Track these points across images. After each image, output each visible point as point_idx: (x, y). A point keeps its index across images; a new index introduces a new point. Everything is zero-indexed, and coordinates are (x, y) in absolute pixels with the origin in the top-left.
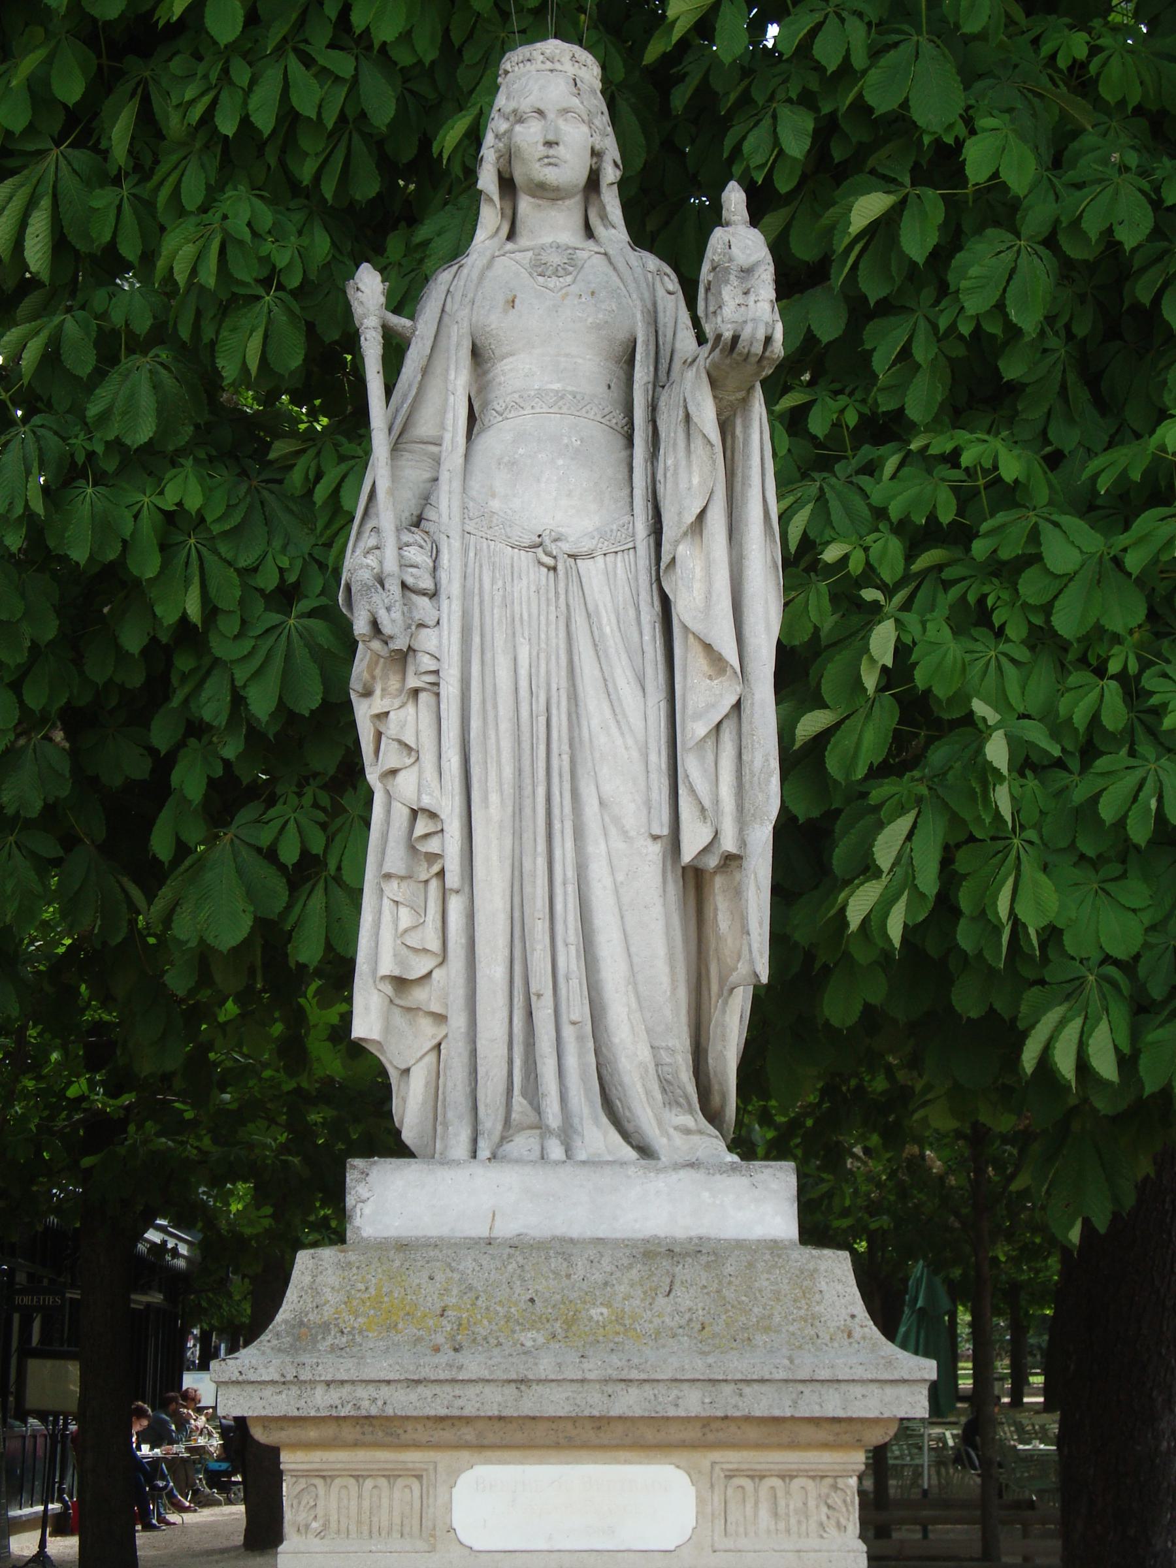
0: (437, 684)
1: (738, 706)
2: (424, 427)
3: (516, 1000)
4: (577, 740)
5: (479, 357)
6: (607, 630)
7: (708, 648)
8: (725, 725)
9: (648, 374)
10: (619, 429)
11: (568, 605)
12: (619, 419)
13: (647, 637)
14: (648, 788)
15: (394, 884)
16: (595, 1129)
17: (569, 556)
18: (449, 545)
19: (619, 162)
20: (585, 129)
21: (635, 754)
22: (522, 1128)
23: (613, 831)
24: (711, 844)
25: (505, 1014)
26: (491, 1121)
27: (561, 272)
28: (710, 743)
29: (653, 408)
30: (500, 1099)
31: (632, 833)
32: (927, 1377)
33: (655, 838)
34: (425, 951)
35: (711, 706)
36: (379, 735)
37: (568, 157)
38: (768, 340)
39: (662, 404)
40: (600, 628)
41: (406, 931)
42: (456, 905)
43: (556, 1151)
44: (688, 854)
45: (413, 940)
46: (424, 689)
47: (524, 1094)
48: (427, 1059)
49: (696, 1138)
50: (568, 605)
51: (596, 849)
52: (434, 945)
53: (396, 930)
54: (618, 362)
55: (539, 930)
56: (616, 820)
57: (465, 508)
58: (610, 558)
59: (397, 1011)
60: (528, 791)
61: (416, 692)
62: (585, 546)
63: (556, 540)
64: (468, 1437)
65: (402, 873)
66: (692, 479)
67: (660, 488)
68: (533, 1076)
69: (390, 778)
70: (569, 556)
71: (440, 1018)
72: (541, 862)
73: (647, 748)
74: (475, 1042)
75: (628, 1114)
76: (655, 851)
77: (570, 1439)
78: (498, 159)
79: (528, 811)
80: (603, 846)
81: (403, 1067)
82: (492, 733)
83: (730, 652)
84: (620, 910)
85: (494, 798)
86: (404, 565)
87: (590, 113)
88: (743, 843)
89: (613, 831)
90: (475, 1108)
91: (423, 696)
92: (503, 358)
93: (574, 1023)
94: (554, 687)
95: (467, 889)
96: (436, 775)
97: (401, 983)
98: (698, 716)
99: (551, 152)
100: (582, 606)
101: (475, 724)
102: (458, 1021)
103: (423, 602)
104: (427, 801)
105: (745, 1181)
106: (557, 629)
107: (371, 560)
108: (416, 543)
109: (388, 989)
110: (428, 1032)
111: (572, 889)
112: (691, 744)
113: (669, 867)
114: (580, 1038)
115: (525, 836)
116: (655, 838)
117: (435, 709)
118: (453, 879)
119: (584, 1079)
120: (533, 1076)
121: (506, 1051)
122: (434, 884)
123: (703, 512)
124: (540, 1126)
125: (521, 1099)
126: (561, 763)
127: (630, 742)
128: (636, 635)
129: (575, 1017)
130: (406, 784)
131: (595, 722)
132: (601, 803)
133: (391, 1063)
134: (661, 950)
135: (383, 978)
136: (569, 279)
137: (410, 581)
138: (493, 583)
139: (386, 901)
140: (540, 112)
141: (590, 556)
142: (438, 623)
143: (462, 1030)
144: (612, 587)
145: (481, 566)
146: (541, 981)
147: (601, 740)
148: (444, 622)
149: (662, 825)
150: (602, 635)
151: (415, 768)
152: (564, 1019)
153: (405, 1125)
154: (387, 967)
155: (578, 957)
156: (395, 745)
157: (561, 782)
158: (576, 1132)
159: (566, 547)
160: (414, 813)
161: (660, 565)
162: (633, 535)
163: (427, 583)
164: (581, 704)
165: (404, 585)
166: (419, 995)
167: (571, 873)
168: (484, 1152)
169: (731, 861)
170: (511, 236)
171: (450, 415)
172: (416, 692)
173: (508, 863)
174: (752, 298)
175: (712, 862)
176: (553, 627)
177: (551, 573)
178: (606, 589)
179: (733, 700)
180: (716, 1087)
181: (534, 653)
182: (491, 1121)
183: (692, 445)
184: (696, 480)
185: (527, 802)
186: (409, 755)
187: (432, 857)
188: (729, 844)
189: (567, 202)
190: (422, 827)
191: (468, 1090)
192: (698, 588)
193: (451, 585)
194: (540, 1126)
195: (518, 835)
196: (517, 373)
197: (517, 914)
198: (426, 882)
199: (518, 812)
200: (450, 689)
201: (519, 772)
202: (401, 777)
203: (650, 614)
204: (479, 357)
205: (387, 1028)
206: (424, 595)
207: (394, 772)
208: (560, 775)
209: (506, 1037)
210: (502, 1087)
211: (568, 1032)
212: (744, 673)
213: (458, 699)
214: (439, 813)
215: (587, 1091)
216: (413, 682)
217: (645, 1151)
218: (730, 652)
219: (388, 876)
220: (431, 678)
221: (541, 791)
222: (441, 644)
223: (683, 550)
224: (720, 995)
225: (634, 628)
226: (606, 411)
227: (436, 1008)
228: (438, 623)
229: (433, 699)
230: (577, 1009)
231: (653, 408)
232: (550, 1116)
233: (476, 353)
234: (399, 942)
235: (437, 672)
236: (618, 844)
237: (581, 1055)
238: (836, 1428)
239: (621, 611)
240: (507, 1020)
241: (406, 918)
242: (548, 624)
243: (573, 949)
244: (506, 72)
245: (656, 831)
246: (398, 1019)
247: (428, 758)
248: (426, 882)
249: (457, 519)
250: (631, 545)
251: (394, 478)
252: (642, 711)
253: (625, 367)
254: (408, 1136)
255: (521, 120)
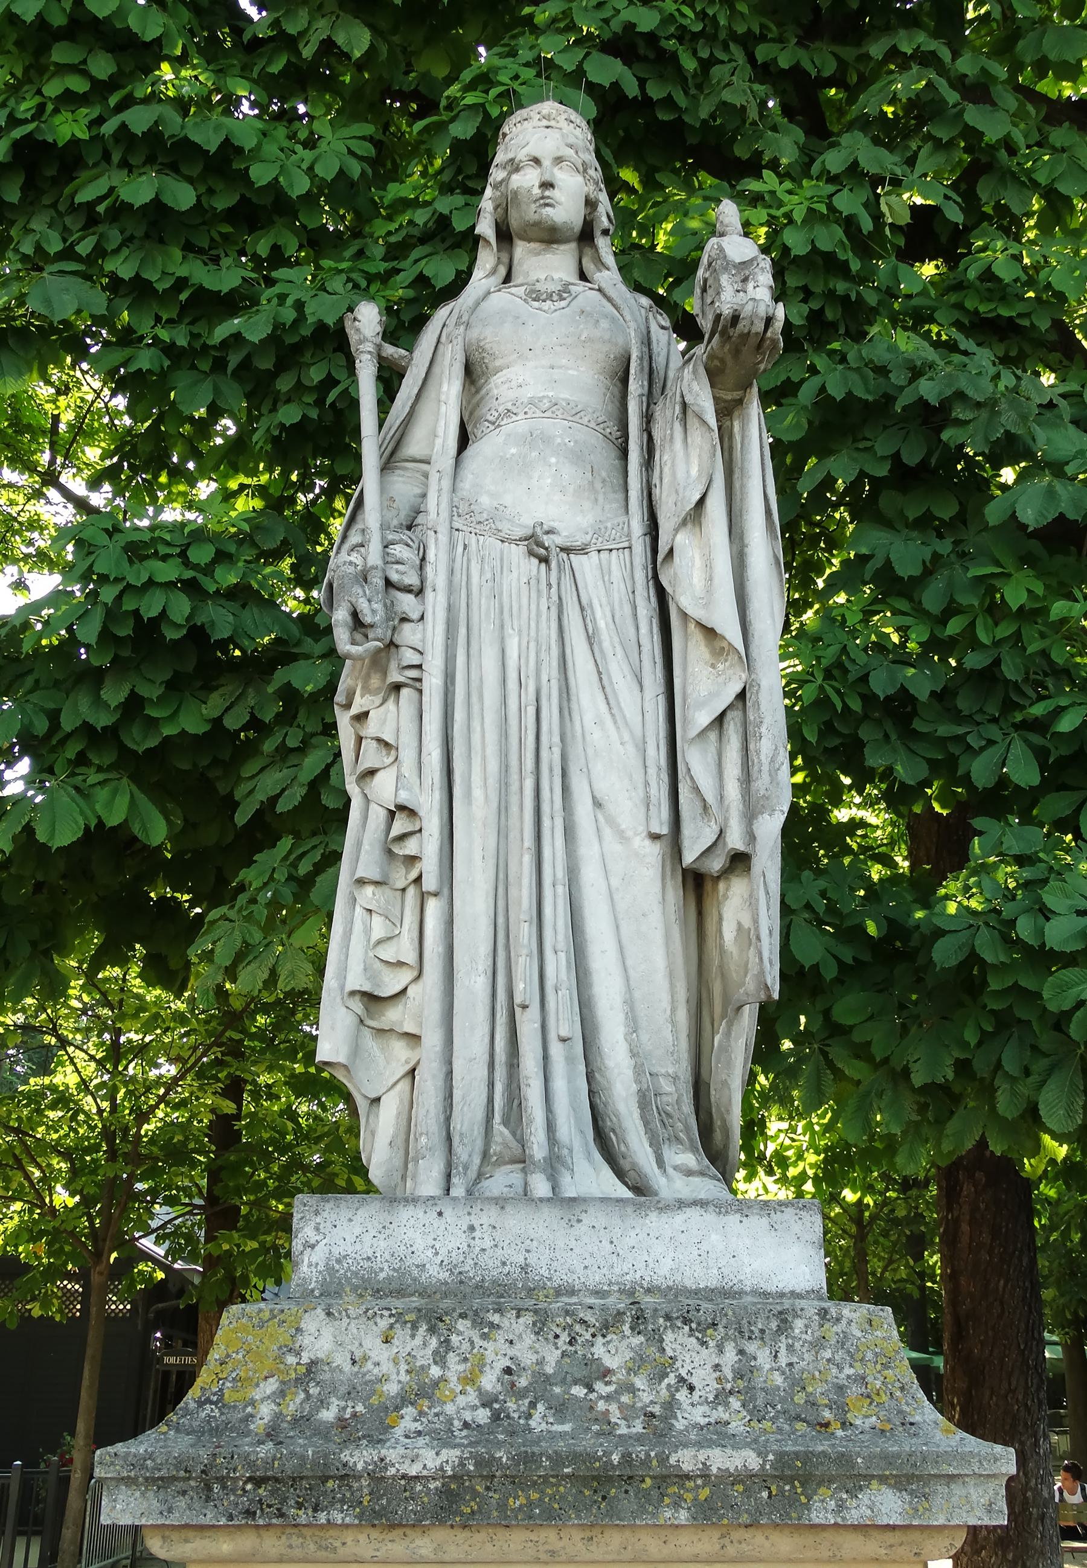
0: (420, 680)
1: (742, 696)
2: (414, 447)
3: (498, 1015)
4: (569, 734)
5: (473, 373)
6: (601, 624)
7: (710, 633)
8: (730, 715)
9: (642, 386)
10: (613, 438)
11: (560, 598)
12: (613, 429)
13: (644, 630)
14: (647, 784)
15: (369, 890)
16: (586, 1164)
17: (562, 549)
18: (436, 540)
19: (612, 214)
20: (580, 179)
21: (631, 749)
22: (501, 1162)
23: (607, 832)
24: (715, 844)
25: (486, 1029)
26: (467, 1152)
27: (555, 297)
28: (713, 736)
29: (648, 419)
30: (478, 1132)
31: (630, 833)
32: (1004, 1470)
33: (655, 837)
34: (400, 964)
35: (713, 695)
36: (360, 740)
37: (563, 199)
38: (769, 321)
39: (657, 415)
40: (594, 620)
41: (379, 942)
42: (433, 907)
43: (541, 1187)
44: (689, 857)
45: (388, 953)
46: (405, 685)
47: (506, 1122)
48: (399, 1087)
49: (696, 1180)
50: (560, 598)
51: (588, 850)
52: (411, 957)
53: (369, 941)
54: (612, 378)
55: (524, 933)
56: (611, 822)
57: (453, 506)
58: (604, 555)
59: (366, 1032)
60: (515, 787)
61: (397, 687)
62: (579, 540)
63: (547, 533)
64: (423, 1552)
65: (377, 877)
66: (686, 464)
67: (656, 492)
68: (516, 1102)
69: (368, 780)
70: (562, 549)
71: (413, 1039)
72: (528, 859)
73: (645, 742)
74: (451, 1063)
75: (623, 1148)
76: (654, 852)
77: (552, 1553)
78: (496, 209)
79: (514, 809)
80: (596, 847)
81: (373, 1095)
82: (476, 725)
83: (732, 633)
84: (616, 918)
85: (478, 793)
86: (388, 560)
87: (584, 163)
88: (751, 837)
89: (607, 832)
90: (449, 1139)
91: (405, 692)
92: (498, 370)
93: (564, 1040)
94: (544, 678)
95: (446, 891)
96: (415, 772)
97: (372, 1000)
98: (701, 705)
99: (547, 193)
100: (575, 598)
101: (459, 715)
102: (432, 1039)
103: (409, 598)
104: (404, 797)
105: (765, 1221)
106: (548, 620)
107: (355, 557)
108: (401, 542)
109: (357, 1005)
110: (401, 1055)
111: (561, 890)
112: (693, 732)
113: (669, 873)
114: (570, 1060)
115: (511, 835)
116: (655, 837)
117: (417, 705)
118: (430, 883)
119: (574, 1107)
120: (516, 1102)
121: (486, 1073)
122: (411, 891)
123: (701, 502)
124: (522, 1160)
125: (502, 1128)
126: (551, 756)
127: (626, 737)
128: (632, 631)
129: (564, 1033)
130: (385, 788)
131: (589, 718)
132: (597, 804)
133: (359, 1091)
134: (659, 960)
135: (353, 993)
136: (563, 303)
137: (394, 577)
138: (482, 572)
139: (358, 909)
140: (537, 161)
141: (583, 550)
142: (422, 618)
143: (438, 1049)
144: (609, 583)
145: (469, 560)
146: (525, 988)
147: (596, 736)
148: (429, 617)
149: (661, 824)
150: (596, 628)
151: (395, 768)
152: (552, 1036)
153: (374, 1161)
154: (356, 981)
155: (568, 967)
156: (374, 744)
157: (551, 776)
158: (564, 1164)
159: (559, 540)
160: (392, 814)
161: (658, 556)
162: (629, 535)
163: (412, 579)
164: (573, 698)
165: (388, 583)
166: (392, 1016)
167: (561, 874)
168: (458, 1191)
169: (740, 861)
170: (507, 279)
171: (442, 423)
172: (397, 687)
173: (492, 862)
174: (750, 285)
175: (716, 864)
176: (544, 617)
177: (543, 565)
178: (600, 583)
179: (738, 688)
180: (718, 1123)
181: (524, 644)
182: (467, 1152)
183: (689, 440)
184: (694, 471)
185: (514, 800)
186: (388, 754)
187: (412, 860)
188: (735, 841)
189: (562, 247)
190: (400, 826)
191: (442, 1118)
192: (697, 579)
193: (437, 575)
194: (522, 1160)
195: (502, 833)
196: (513, 383)
197: (501, 920)
198: (404, 890)
199: (503, 810)
200: (433, 682)
201: (505, 768)
202: (379, 776)
203: (646, 609)
204: (473, 373)
205: (356, 1050)
206: (410, 591)
207: (372, 772)
208: (551, 770)
209: (486, 1057)
210: (480, 1114)
211: (556, 1050)
212: (748, 661)
213: (441, 691)
214: (416, 809)
215: (578, 1120)
216: (395, 677)
217: (640, 1189)
218: (732, 633)
219: (361, 882)
220: (414, 674)
221: (529, 784)
222: (425, 639)
223: (682, 540)
224: (724, 1016)
225: (629, 621)
226: (600, 420)
227: (409, 1028)
228: (422, 618)
229: (414, 694)
230: (565, 1021)
231: (648, 419)
232: (535, 1147)
233: (469, 371)
234: (371, 954)
235: (419, 667)
236: (613, 846)
237: (570, 1080)
238: (891, 1538)
239: (617, 607)
240: (487, 1040)
241: (379, 928)
242: (538, 615)
243: (562, 956)
244: (505, 135)
245: (656, 829)
246: (369, 1041)
247: (407, 755)
248: (404, 890)
249: (445, 514)
250: (626, 544)
251: (383, 489)
252: (642, 706)
253: (619, 384)
254: (375, 1174)
255: (517, 169)
